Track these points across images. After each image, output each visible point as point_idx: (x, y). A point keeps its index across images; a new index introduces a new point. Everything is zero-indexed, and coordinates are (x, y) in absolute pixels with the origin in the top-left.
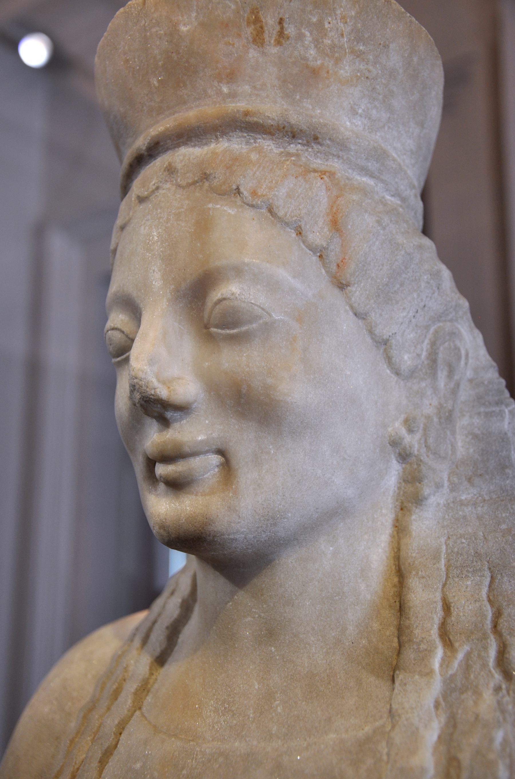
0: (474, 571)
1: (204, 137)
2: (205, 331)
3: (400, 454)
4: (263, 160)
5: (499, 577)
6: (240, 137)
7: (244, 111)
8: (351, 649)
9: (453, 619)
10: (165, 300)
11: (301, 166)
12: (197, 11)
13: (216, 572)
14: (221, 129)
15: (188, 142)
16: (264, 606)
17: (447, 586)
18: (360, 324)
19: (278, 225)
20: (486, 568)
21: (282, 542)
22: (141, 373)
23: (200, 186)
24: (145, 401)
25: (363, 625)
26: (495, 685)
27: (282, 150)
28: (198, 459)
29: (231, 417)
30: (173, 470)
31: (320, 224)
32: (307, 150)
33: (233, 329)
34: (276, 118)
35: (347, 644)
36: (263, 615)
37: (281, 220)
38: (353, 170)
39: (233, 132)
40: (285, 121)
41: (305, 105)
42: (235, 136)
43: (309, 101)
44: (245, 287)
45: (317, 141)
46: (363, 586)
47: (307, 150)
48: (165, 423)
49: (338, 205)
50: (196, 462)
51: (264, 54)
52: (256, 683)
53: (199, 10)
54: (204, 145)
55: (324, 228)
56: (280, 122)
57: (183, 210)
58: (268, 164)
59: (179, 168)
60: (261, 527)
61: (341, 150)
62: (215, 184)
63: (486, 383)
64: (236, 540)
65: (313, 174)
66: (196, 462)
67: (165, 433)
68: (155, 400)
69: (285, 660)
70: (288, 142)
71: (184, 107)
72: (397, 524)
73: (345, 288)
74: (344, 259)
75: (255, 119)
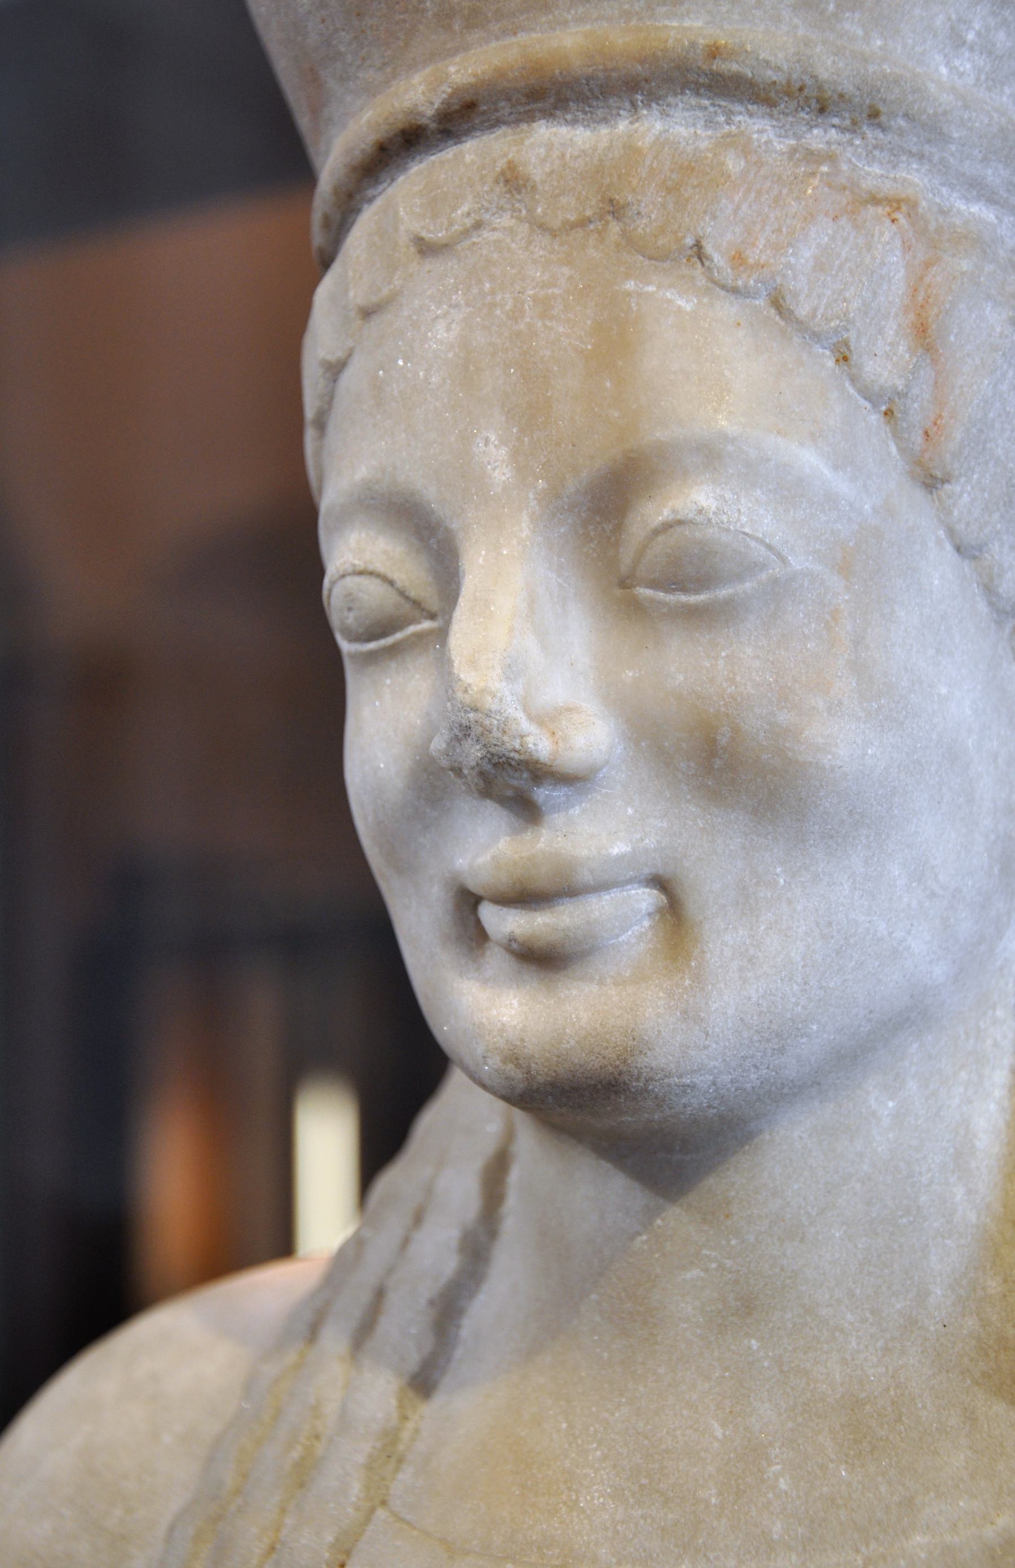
1: (601, 104)
2: (618, 592)
4: (755, 175)
6: (692, 108)
7: (708, 46)
8: (942, 1340)
10: (525, 517)
11: (845, 188)
13: (603, 1162)
14: (647, 87)
15: (558, 113)
16: (733, 1242)
18: (966, 569)
19: (796, 339)
21: (786, 1090)
22: (489, 698)
23: (599, 233)
24: (495, 765)
25: (964, 1282)
27: (793, 142)
28: (606, 897)
29: (688, 801)
31: (890, 333)
32: (850, 143)
33: (696, 591)
34: (785, 67)
35: (932, 1328)
36: (728, 1263)
37: (801, 326)
38: (952, 187)
39: (676, 95)
40: (805, 72)
41: (847, 26)
42: (680, 105)
43: (857, 15)
44: (728, 495)
45: (877, 121)
46: (959, 1193)
47: (850, 143)
48: (526, 810)
49: (929, 286)
50: (603, 907)
52: (716, 1426)
54: (599, 122)
55: (898, 344)
56: (795, 76)
57: (556, 291)
58: (768, 184)
59: (538, 179)
60: (752, 1057)
61: (929, 141)
62: (640, 230)
64: (693, 1087)
65: (871, 210)
66: (603, 907)
67: (528, 836)
68: (520, 762)
69: (785, 1369)
70: (808, 124)
73: (939, 486)
74: (940, 416)
75: (735, 67)
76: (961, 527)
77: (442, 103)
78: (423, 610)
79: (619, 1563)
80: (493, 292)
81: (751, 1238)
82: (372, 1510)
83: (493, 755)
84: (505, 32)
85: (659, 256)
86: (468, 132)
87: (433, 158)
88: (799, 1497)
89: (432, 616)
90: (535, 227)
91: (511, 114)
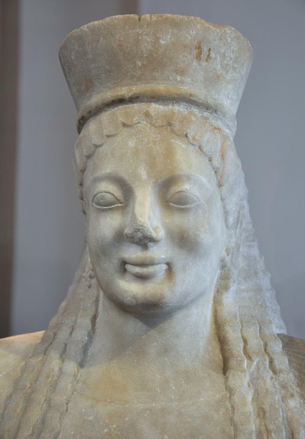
0: (253, 324)
2: (165, 203)
3: (222, 266)
5: (263, 327)
6: (184, 105)
9: (249, 346)
10: (150, 186)
12: (171, 35)
14: (177, 100)
15: (157, 102)
16: (165, 338)
17: (243, 331)
20: (257, 323)
24: (144, 238)
26: (270, 376)
27: (201, 114)
29: (176, 248)
30: (146, 271)
33: (183, 206)
39: (182, 102)
40: (206, 101)
41: (212, 92)
44: (191, 187)
48: (145, 247)
51: (200, 65)
52: (158, 376)
53: (172, 35)
56: (204, 102)
61: (223, 117)
62: (175, 130)
63: (250, 230)
67: (144, 252)
71: (155, 82)
72: (214, 299)
74: (223, 173)
75: (194, 99)
76: (223, 195)
78: (120, 201)
80: (142, 138)
81: (168, 337)
82: (73, 392)
83: (144, 236)
84: (146, 83)
85: (178, 135)
86: (135, 102)
87: (126, 106)
89: (121, 203)
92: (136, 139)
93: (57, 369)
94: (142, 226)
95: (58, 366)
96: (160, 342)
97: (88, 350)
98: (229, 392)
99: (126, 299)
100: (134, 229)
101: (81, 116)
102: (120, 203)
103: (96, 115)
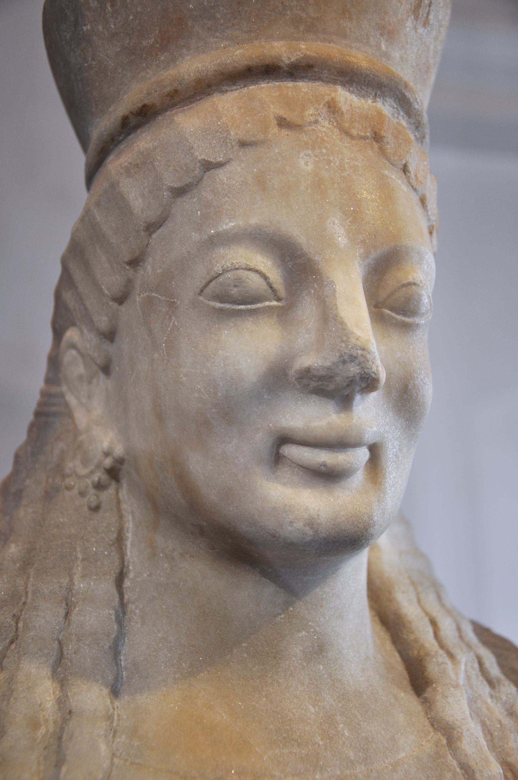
1: (365, 89)
15: (347, 85)
30: (345, 460)
33: (409, 317)
48: (345, 402)
52: (310, 707)
67: (343, 415)
77: (297, 60)
79: (285, 776)
86: (302, 78)
87: (278, 83)
88: (355, 739)
89: (279, 300)
90: (342, 132)
91: (327, 77)
92: (316, 156)
93: (51, 703)
94: (363, 349)
95: (52, 697)
96: (312, 630)
97: (120, 653)
98: (441, 733)
99: (290, 528)
100: (341, 356)
101: (143, 103)
102: (275, 300)
103: (191, 103)
